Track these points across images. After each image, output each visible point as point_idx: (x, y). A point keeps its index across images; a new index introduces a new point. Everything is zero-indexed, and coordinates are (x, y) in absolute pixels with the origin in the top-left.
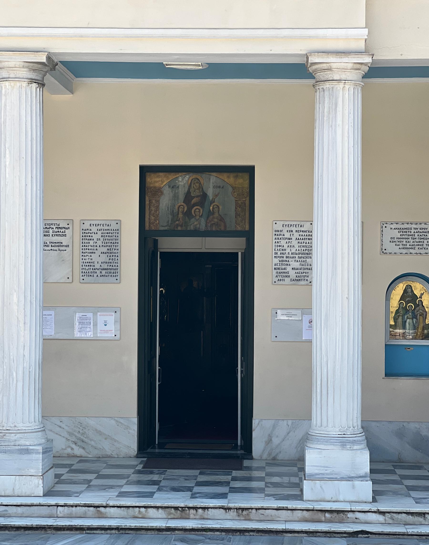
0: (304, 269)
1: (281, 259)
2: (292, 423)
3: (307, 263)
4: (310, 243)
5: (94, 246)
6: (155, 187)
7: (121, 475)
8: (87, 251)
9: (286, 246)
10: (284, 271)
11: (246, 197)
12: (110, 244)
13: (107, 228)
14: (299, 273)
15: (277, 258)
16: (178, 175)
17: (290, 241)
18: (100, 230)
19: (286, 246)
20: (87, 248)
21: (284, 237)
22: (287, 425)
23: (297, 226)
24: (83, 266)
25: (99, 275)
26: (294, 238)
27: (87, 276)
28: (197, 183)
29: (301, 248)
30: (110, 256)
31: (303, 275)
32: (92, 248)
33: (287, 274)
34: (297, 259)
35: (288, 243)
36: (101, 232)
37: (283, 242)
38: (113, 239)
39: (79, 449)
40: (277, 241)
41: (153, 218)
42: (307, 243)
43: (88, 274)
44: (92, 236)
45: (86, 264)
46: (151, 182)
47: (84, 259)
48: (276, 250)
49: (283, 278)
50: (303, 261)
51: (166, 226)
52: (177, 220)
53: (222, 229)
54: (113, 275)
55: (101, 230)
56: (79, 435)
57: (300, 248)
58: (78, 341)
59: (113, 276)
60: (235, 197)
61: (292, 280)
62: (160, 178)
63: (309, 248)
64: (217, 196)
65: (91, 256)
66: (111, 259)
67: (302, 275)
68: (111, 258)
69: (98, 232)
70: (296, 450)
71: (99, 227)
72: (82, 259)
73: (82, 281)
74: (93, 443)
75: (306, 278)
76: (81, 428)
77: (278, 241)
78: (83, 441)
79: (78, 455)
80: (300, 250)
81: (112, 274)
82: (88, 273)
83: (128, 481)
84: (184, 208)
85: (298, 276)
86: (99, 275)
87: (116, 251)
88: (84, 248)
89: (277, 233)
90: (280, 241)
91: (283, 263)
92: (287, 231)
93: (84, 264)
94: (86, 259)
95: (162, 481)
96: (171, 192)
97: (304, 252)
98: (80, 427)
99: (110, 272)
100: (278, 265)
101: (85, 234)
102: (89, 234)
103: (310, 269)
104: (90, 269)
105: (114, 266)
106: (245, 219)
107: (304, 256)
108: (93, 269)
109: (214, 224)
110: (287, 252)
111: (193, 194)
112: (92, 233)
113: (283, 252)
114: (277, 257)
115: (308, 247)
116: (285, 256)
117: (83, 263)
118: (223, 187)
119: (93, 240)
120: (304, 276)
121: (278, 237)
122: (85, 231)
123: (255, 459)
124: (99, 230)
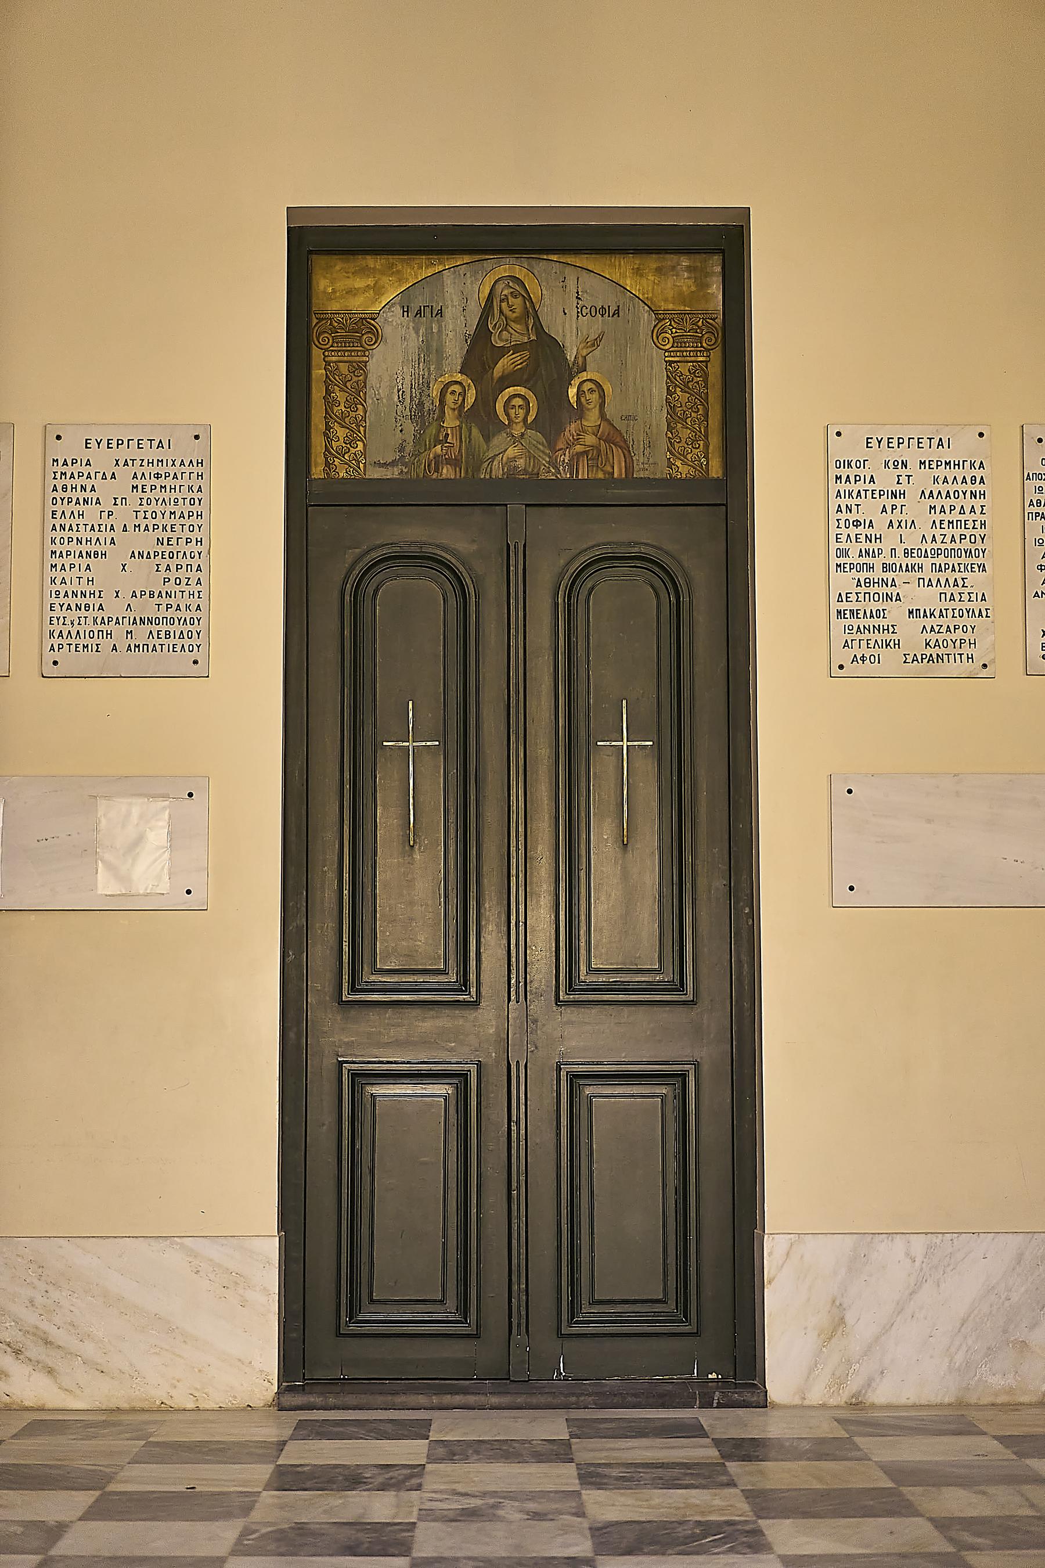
0: (956, 614)
1: (863, 576)
2: (929, 1247)
3: (966, 590)
4: (978, 510)
5: (103, 528)
6: (349, 312)
7: (213, 1494)
8: (73, 547)
9: (881, 522)
10: (876, 622)
11: (708, 350)
12: (168, 521)
13: (154, 454)
14: (937, 629)
15: (848, 569)
16: (440, 264)
17: (898, 502)
18: (126, 464)
19: (881, 522)
20: (71, 534)
21: (871, 487)
22: (907, 1254)
23: (925, 442)
24: (57, 607)
25: (122, 647)
26: (912, 491)
27: (73, 647)
28: (516, 298)
29: (943, 532)
30: (168, 568)
31: (954, 637)
32: (94, 535)
33: (888, 637)
34: (927, 574)
35: (889, 510)
36: (131, 470)
37: (869, 509)
38: (181, 501)
39: (30, 1376)
40: (844, 502)
41: (341, 433)
42: (967, 510)
43: (74, 642)
44: (93, 489)
45: (66, 601)
46: (334, 291)
47: (58, 581)
48: (844, 538)
49: (871, 651)
50: (952, 582)
51: (393, 463)
52: (437, 442)
53: (616, 476)
54: (179, 643)
55: (130, 463)
56: (31, 1318)
57: (938, 532)
58: (33, 917)
59: (178, 648)
60: (666, 351)
61: (910, 660)
62: (368, 276)
63: (974, 532)
64: (596, 343)
65: (88, 567)
66: (172, 581)
67: (949, 637)
68: (173, 575)
69: (115, 470)
70: (947, 1360)
71: (123, 453)
72: (53, 581)
73: (49, 669)
74: (89, 1349)
75: (966, 650)
76: (42, 1286)
77: (850, 502)
78: (47, 1343)
79: (27, 1403)
80: (939, 539)
81: (177, 641)
82: (74, 635)
83: (246, 1532)
84: (463, 394)
85: (932, 644)
86: (122, 647)
87: (192, 547)
88: (58, 534)
89: (844, 472)
90: (858, 501)
91: (872, 590)
92: (886, 464)
93: (62, 600)
94: (68, 582)
95: (421, 1525)
96: (412, 332)
97: (953, 545)
98: (36, 1281)
99: (168, 634)
100: (853, 597)
101: (64, 481)
102: (83, 481)
103: (980, 614)
104: (83, 620)
105: (183, 607)
106: (706, 436)
107: (957, 560)
108: (99, 621)
109: (586, 453)
110: (886, 546)
111: (501, 340)
112: (93, 476)
113: (871, 546)
114: (847, 566)
115: (970, 525)
116: (877, 562)
117: (54, 595)
118: (617, 313)
119: (98, 502)
120: (958, 643)
121: (848, 487)
122: (64, 469)
123: (775, 1406)
124: (121, 463)
